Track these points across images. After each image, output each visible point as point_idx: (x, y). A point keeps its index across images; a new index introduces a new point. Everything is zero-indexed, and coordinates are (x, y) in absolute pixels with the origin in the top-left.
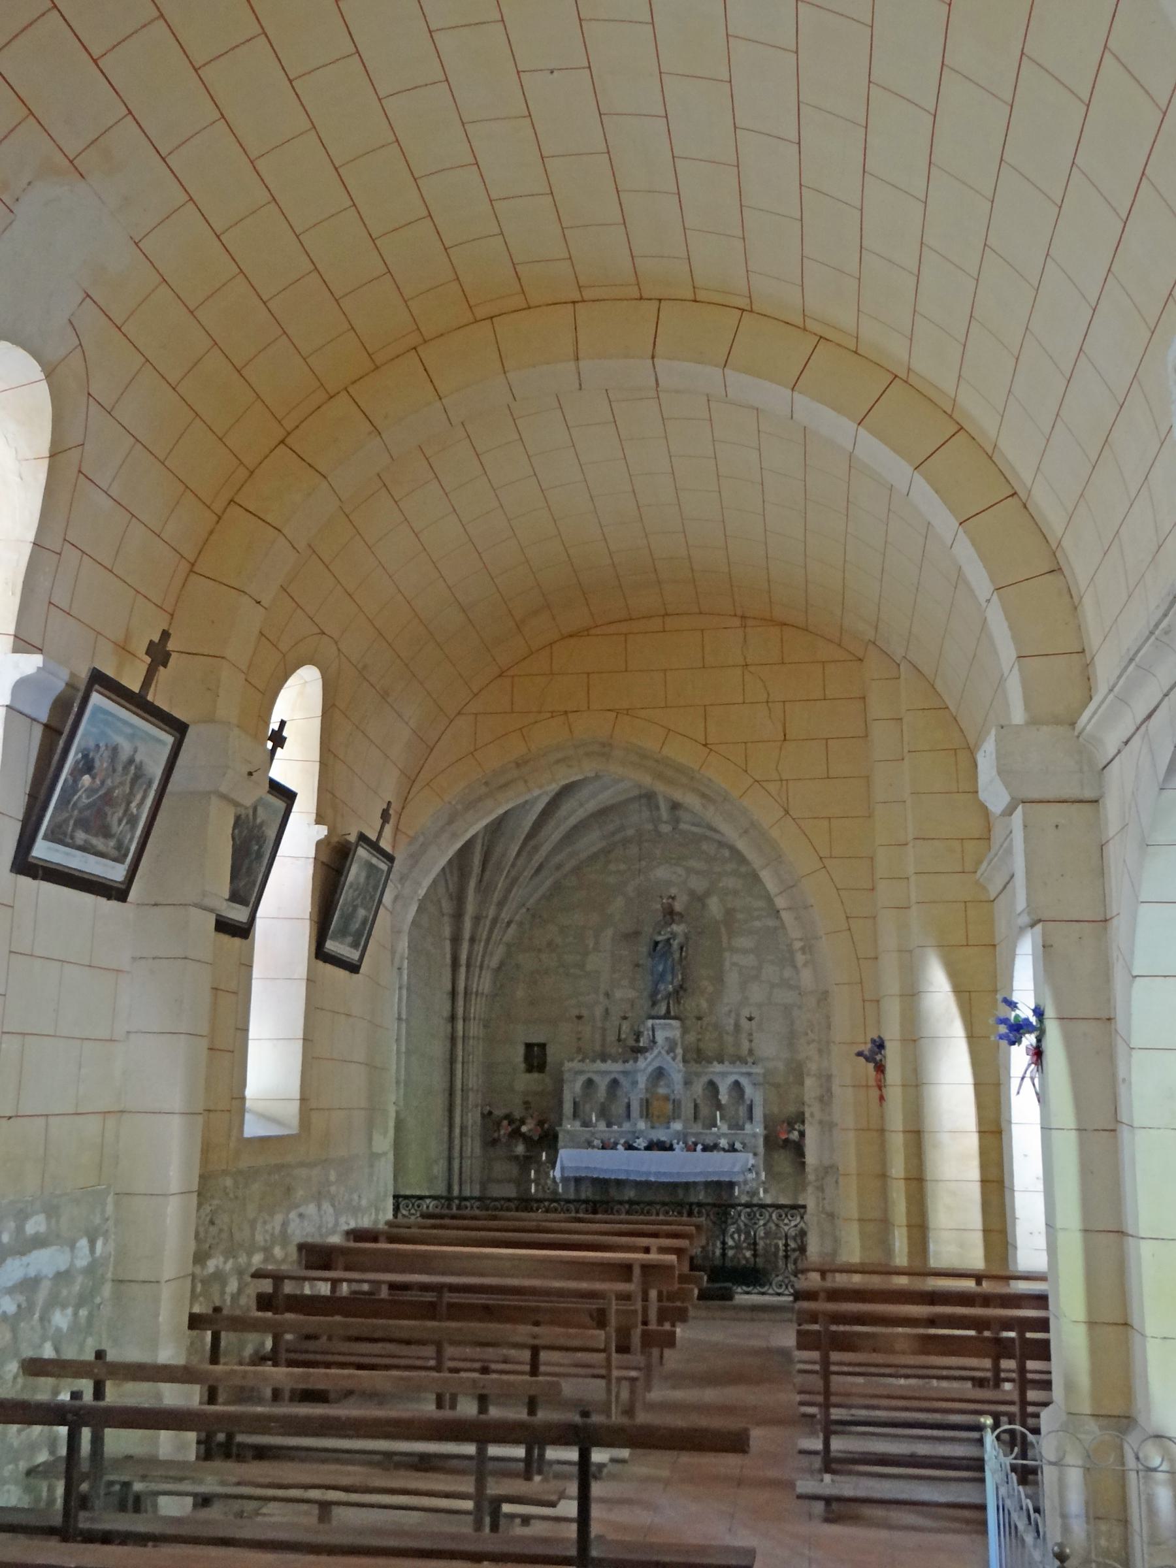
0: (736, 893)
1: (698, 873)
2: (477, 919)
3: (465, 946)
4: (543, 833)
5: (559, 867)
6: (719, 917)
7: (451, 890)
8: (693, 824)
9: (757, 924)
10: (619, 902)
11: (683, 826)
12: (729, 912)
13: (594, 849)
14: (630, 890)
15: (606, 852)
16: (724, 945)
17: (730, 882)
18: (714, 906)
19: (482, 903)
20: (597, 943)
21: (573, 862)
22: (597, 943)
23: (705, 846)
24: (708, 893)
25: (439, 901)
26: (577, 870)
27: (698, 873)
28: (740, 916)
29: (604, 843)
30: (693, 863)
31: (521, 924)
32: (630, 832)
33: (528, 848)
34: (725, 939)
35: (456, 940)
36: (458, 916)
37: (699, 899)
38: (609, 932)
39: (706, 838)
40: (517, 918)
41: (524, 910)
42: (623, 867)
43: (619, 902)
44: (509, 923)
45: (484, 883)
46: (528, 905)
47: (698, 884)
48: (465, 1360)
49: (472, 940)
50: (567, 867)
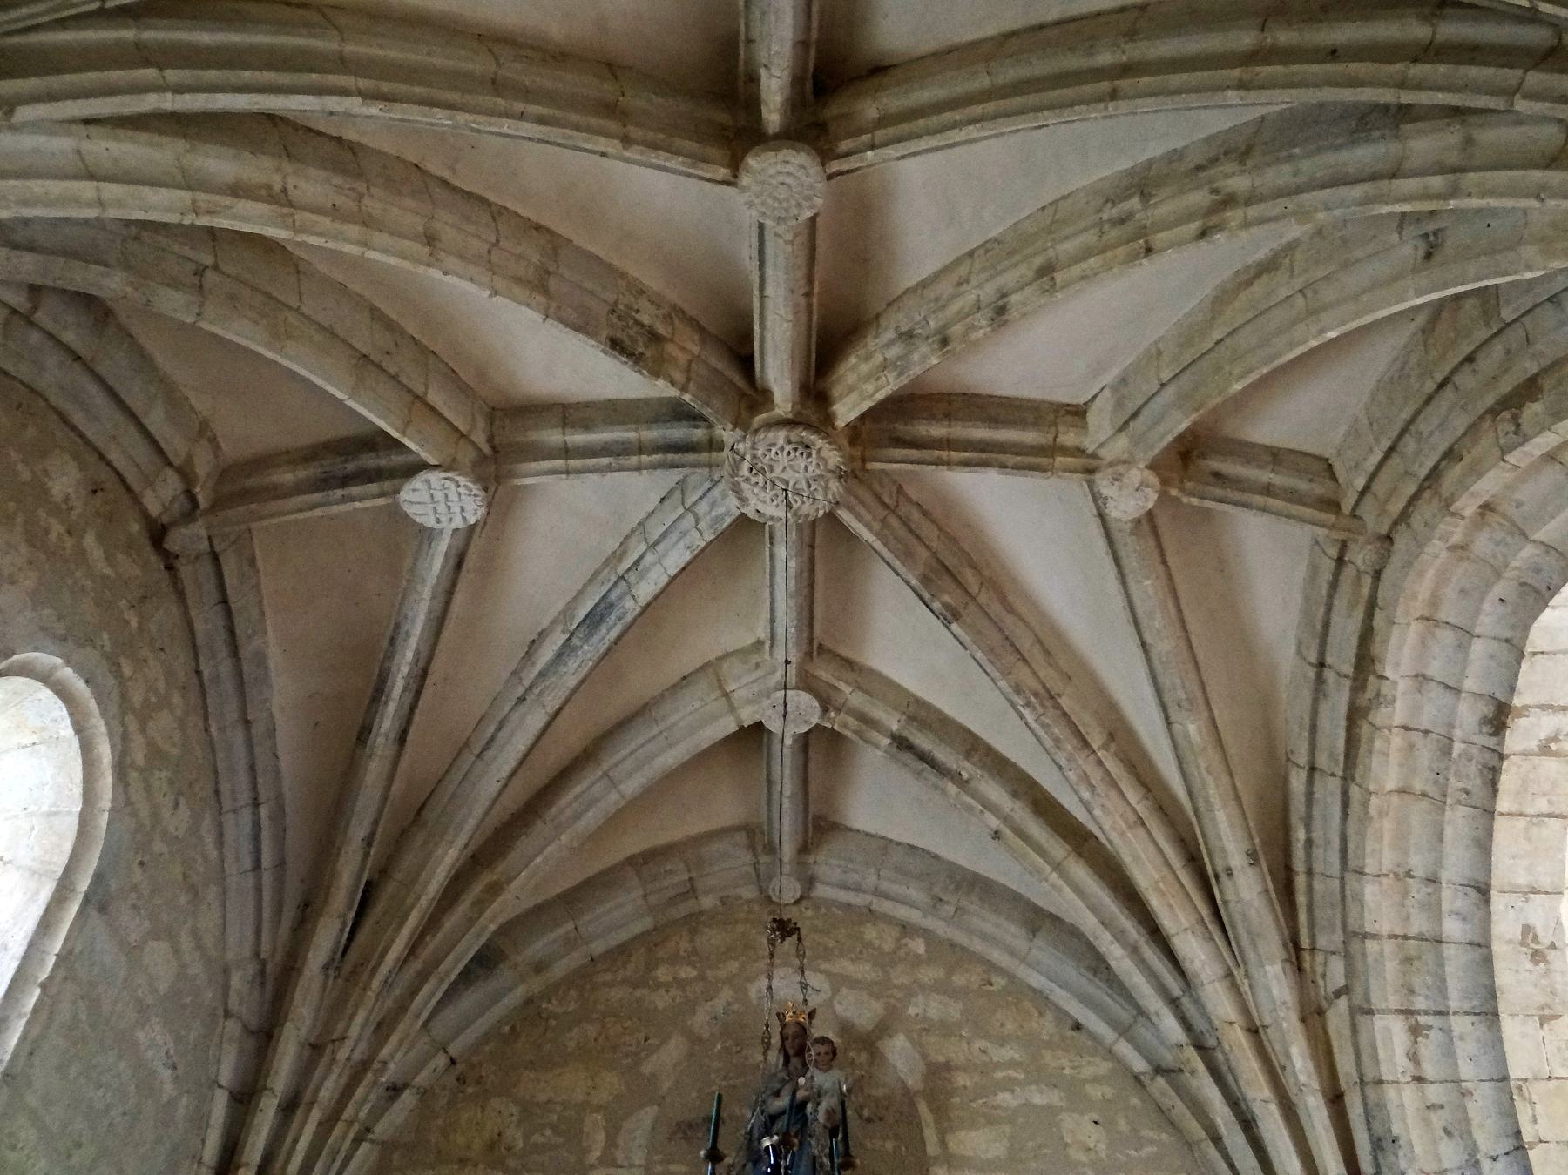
0: (947, 1029)
1: (854, 983)
2: (315, 1049)
3: (268, 1109)
4: (524, 845)
5: (539, 967)
6: (914, 1081)
7: (266, 948)
8: (844, 887)
9: (1004, 1098)
10: (672, 1051)
11: (822, 891)
12: (938, 1073)
13: (623, 936)
14: (700, 1020)
15: (652, 940)
16: (932, 1149)
17: (934, 1007)
18: (900, 1053)
19: (336, 1008)
20: (611, 1143)
21: (576, 958)
22: (611, 1143)
23: (870, 933)
24: (884, 1029)
25: (226, 971)
26: (583, 977)
27: (854, 983)
28: (962, 1080)
29: (646, 923)
30: (845, 966)
31: (425, 1094)
32: (707, 902)
33: (477, 889)
34: (930, 1135)
35: (244, 1099)
36: (265, 1037)
37: (869, 1042)
38: (648, 1115)
39: (871, 915)
40: (422, 1078)
41: (441, 1061)
42: (687, 972)
43: (672, 1051)
44: (395, 1091)
45: (353, 955)
46: (454, 1049)
47: (861, 1011)
48: (1336, 1100)
49: (289, 1107)
50: (559, 970)
